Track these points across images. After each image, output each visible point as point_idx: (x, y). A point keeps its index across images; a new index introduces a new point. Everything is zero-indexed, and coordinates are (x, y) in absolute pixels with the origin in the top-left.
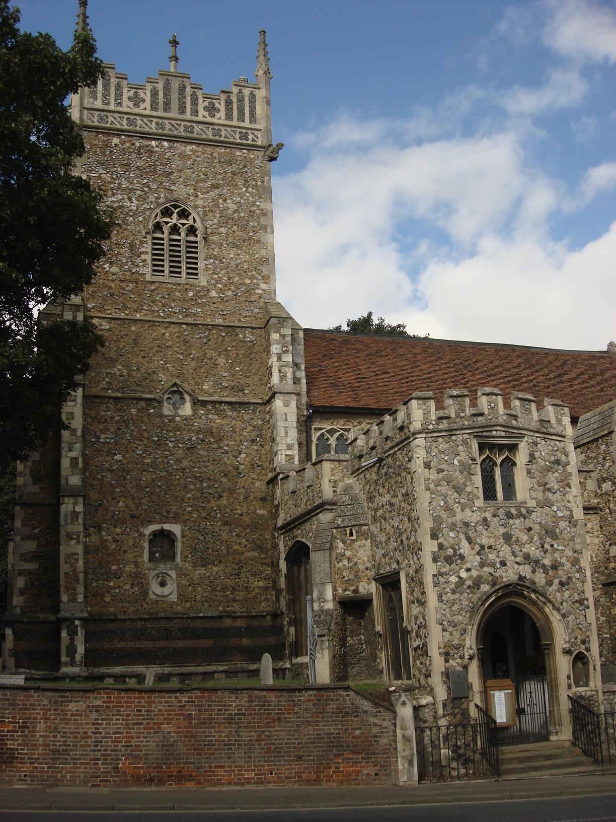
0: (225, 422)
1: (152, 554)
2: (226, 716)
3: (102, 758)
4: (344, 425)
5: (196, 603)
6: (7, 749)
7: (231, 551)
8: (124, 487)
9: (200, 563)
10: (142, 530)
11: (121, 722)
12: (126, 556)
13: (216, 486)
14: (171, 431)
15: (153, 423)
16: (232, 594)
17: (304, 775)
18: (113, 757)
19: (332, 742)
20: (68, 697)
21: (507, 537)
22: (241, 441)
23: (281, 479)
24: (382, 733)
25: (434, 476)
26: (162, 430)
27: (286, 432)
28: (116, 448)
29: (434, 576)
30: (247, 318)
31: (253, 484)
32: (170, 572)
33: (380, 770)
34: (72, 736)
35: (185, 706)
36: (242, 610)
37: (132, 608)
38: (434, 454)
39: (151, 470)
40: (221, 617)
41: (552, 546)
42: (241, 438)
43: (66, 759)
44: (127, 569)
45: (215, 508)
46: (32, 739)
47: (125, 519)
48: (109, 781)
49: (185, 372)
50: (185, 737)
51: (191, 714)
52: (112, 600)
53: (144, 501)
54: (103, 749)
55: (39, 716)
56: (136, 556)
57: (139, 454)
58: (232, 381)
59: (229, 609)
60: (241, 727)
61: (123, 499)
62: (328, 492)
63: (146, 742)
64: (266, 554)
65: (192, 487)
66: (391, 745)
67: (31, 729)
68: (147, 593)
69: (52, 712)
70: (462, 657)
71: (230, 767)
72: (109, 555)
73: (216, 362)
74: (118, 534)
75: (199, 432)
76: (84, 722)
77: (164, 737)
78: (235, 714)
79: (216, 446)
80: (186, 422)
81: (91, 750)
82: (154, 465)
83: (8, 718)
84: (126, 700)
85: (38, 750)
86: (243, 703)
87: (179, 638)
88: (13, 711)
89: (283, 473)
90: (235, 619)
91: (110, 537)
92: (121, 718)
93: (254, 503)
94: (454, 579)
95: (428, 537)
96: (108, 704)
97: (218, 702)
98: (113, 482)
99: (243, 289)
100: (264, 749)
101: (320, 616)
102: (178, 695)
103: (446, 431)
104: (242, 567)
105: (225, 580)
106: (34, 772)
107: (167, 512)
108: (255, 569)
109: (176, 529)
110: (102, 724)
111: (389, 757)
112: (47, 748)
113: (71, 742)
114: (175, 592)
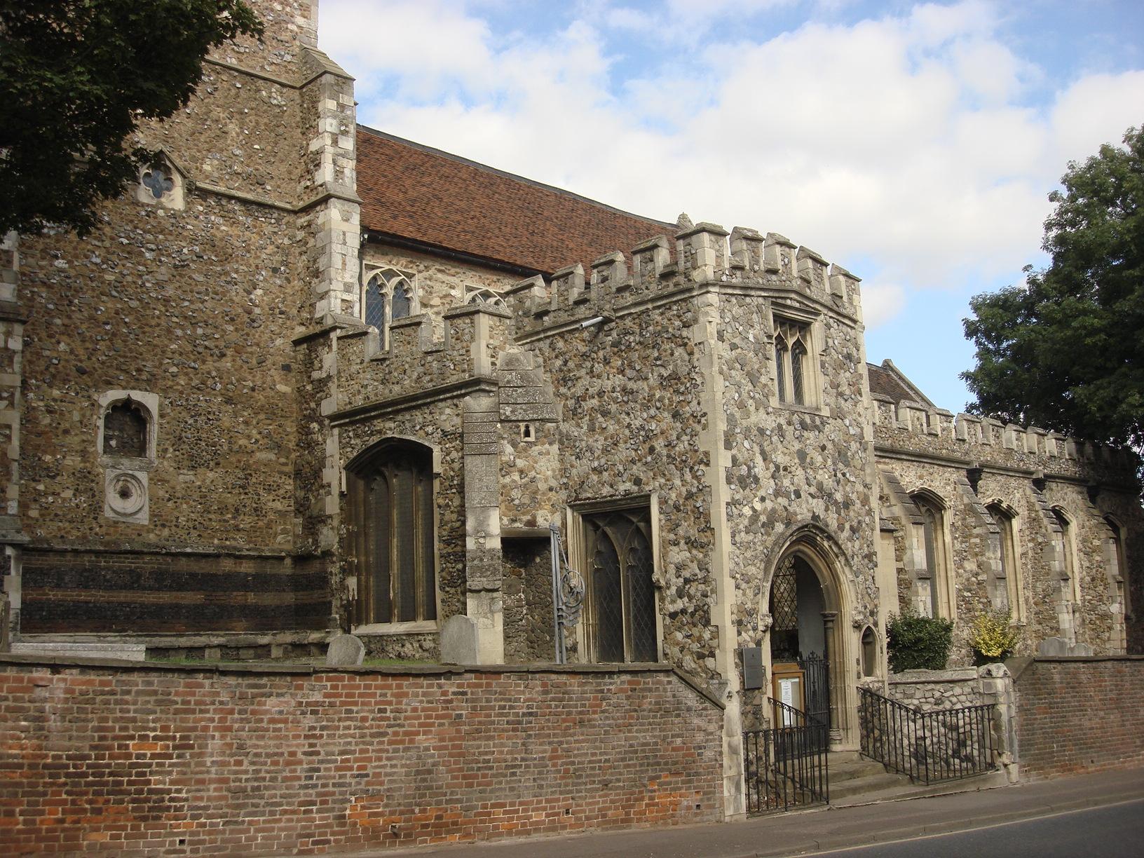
0: (234, 231)
1: (107, 439)
2: (511, 718)
3: (318, 800)
4: (406, 267)
5: (177, 530)
6: (151, 791)
7: (236, 448)
8: (69, 317)
9: (186, 463)
10: (95, 397)
11: (352, 731)
12: (68, 439)
13: (216, 336)
14: (149, 232)
15: (121, 213)
16: (234, 518)
17: (610, 813)
18: (338, 797)
19: (647, 758)
20: (264, 686)
21: (802, 455)
22: (257, 267)
23: (339, 338)
24: (707, 741)
25: (728, 355)
26: (136, 228)
27: (344, 264)
28: (58, 245)
29: (728, 504)
30: (273, 67)
31: (273, 341)
32: (139, 474)
33: (702, 800)
34: (269, 761)
35: (451, 701)
36: (247, 547)
37: (75, 532)
38: (727, 320)
39: (114, 293)
40: (218, 556)
41: (844, 475)
42: (257, 261)
43: (256, 805)
44: (68, 461)
45: (214, 374)
46: (198, 769)
47: (68, 375)
48: (328, 842)
49: (176, 135)
50: (451, 755)
51: (460, 716)
52: (42, 515)
53: (101, 346)
54: (320, 782)
55: (212, 725)
56: (84, 441)
57: (96, 264)
58: (248, 166)
59: (228, 543)
60: (531, 735)
61: (64, 338)
62: (483, 364)
63: (392, 766)
64: (287, 458)
65: (179, 332)
66: (716, 760)
67: (196, 750)
68: (100, 507)
69: (236, 716)
70: (755, 629)
71: (512, 804)
72: (39, 434)
73: (225, 129)
74: (55, 400)
75: (193, 241)
76: (291, 734)
77: (419, 758)
78: (524, 714)
79: (219, 269)
80: (173, 221)
81: (301, 787)
82: (119, 285)
83: (154, 729)
84: (362, 691)
85: (208, 790)
86: (535, 696)
87: (151, 589)
88: (164, 716)
89: (342, 328)
90: (238, 561)
91: (41, 404)
92: (352, 724)
93: (273, 372)
94: (747, 511)
95: (721, 445)
96: (332, 700)
97: (500, 693)
98: (51, 306)
99: (271, 18)
100: (559, 771)
101: (482, 560)
102: (443, 681)
103: (742, 288)
104: (251, 475)
105: (225, 495)
106: (198, 833)
107: (139, 370)
108: (270, 480)
109: (151, 401)
110: (322, 736)
111: (713, 779)
112: (224, 786)
113: (268, 772)
114: (146, 509)
